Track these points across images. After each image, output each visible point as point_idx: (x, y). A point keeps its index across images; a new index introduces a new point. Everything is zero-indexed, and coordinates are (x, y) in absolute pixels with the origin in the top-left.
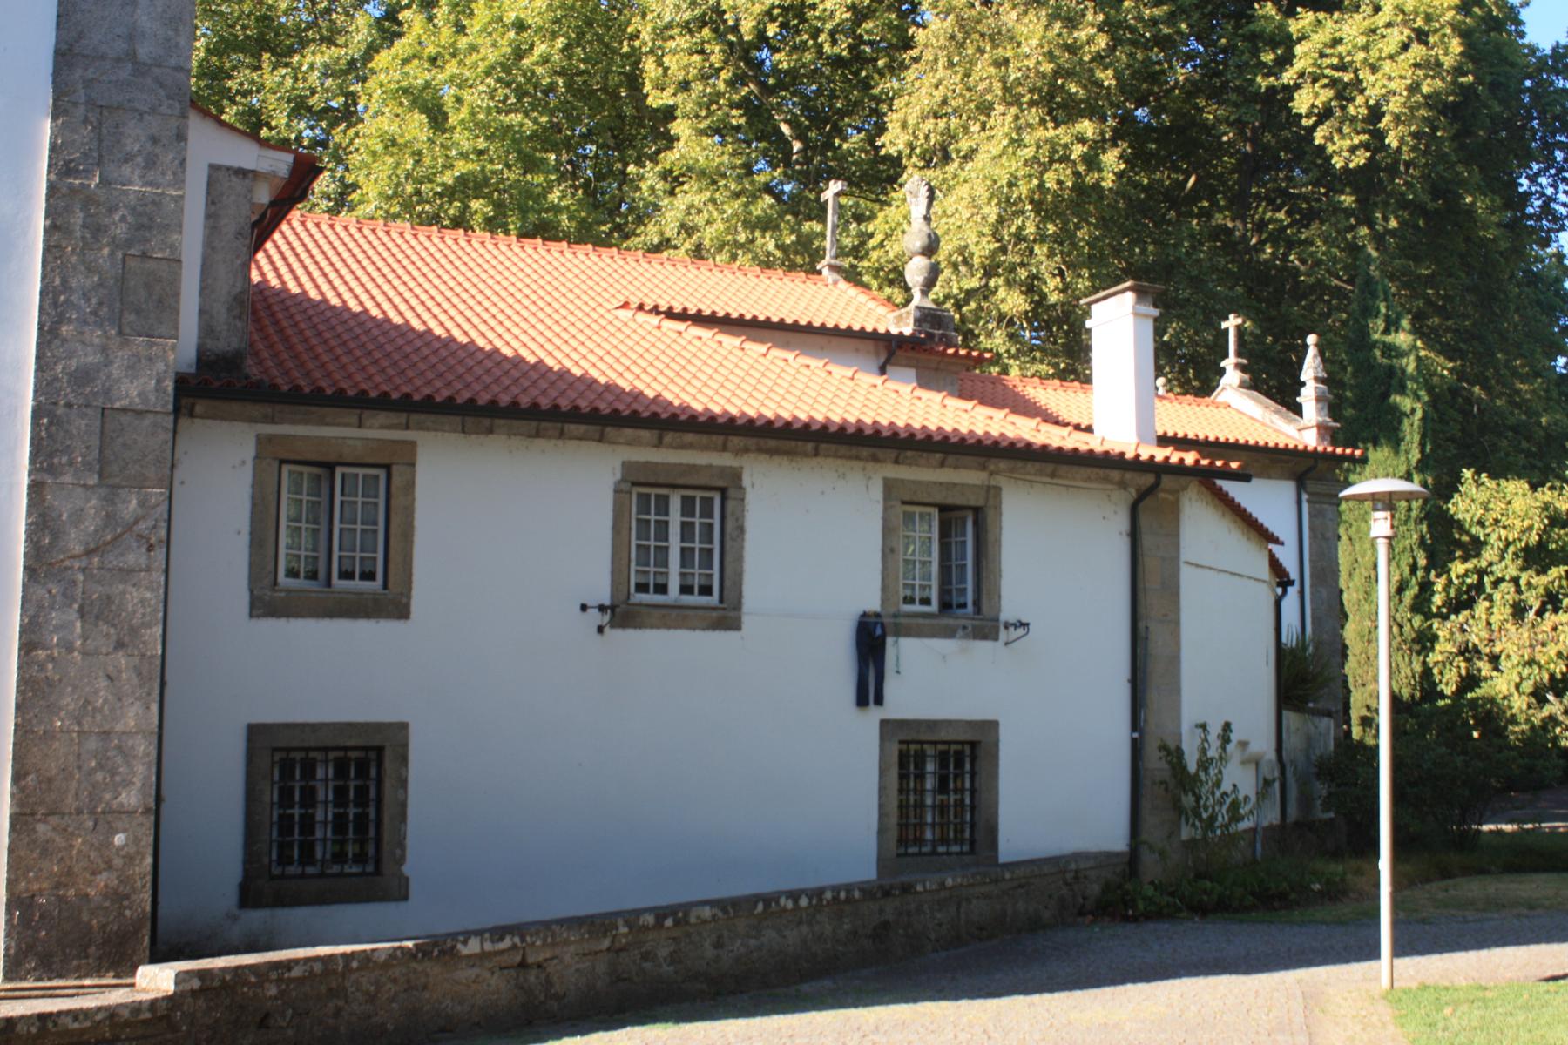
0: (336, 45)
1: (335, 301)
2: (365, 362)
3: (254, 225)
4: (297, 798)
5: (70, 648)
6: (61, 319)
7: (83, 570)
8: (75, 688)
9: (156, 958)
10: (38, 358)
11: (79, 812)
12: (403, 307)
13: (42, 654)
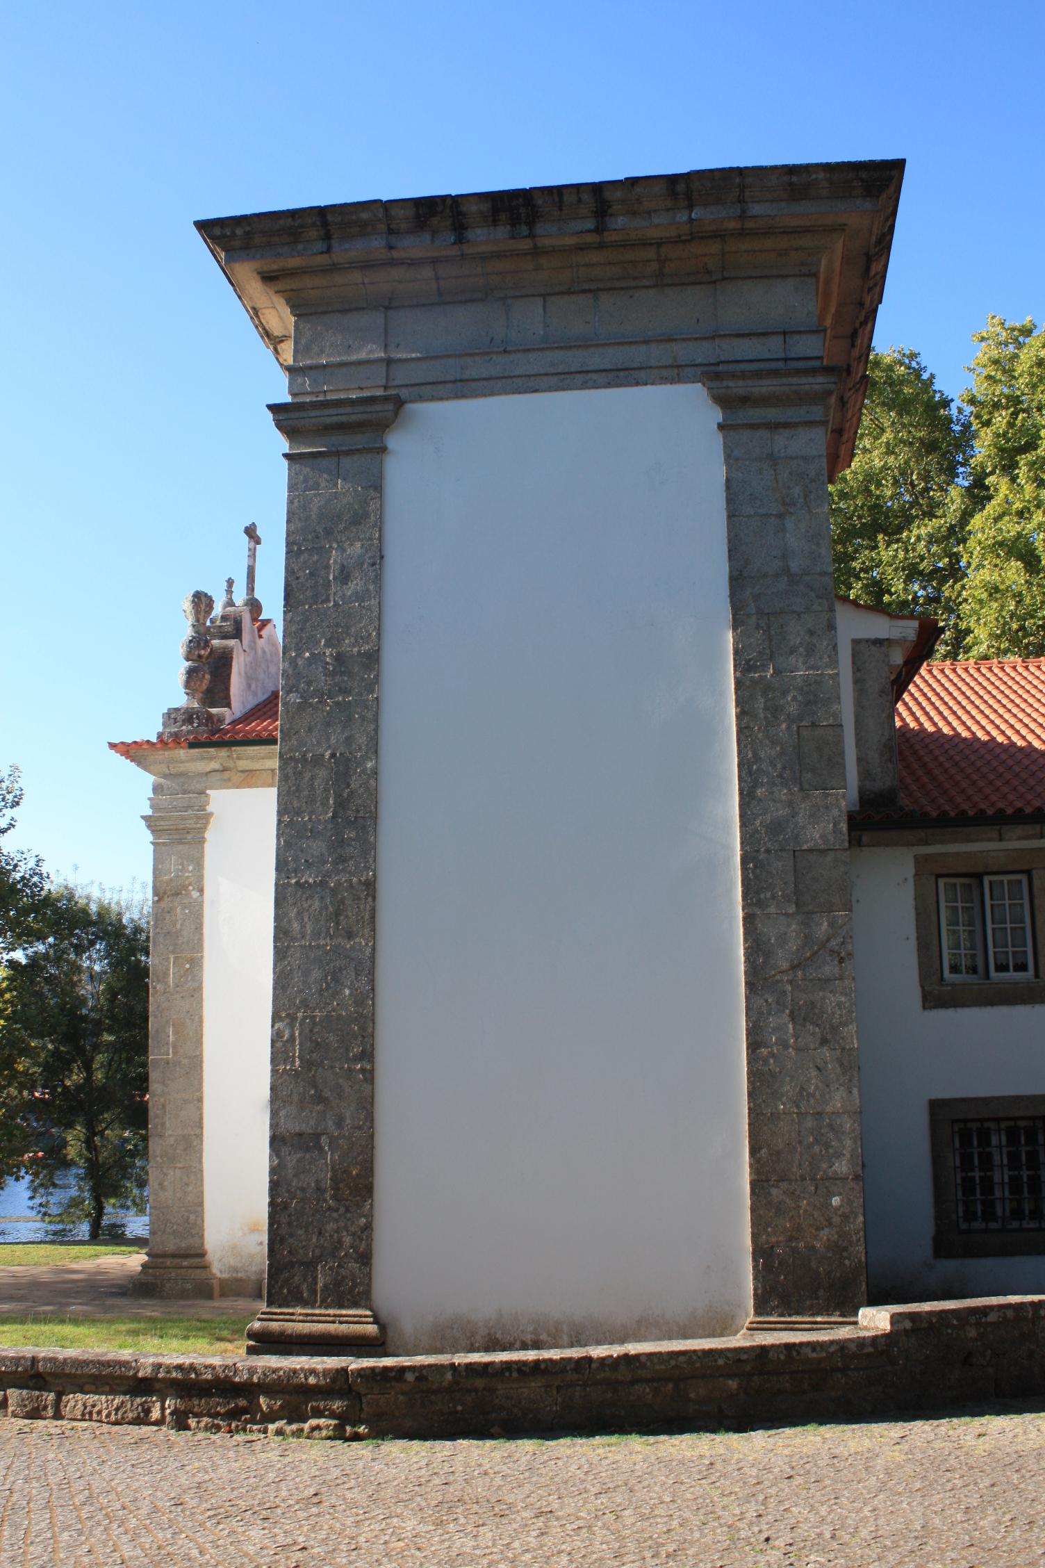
0: (936, 517)
1: (965, 734)
2: (998, 783)
3: (893, 682)
4: (976, 1163)
5: (786, 1046)
6: (756, 784)
7: (791, 982)
8: (792, 1077)
9: (874, 1301)
10: (741, 816)
11: (803, 1179)
12: (1024, 732)
13: (764, 1051)
